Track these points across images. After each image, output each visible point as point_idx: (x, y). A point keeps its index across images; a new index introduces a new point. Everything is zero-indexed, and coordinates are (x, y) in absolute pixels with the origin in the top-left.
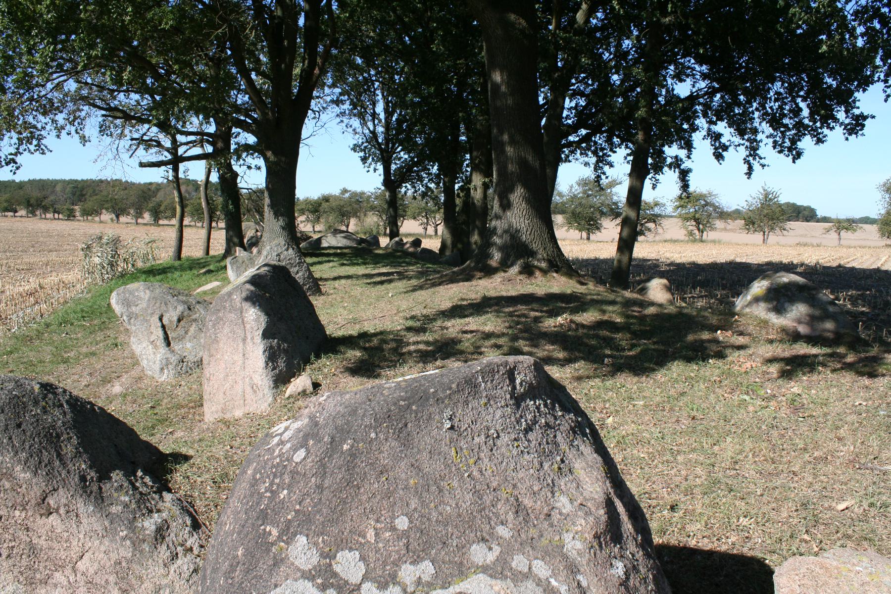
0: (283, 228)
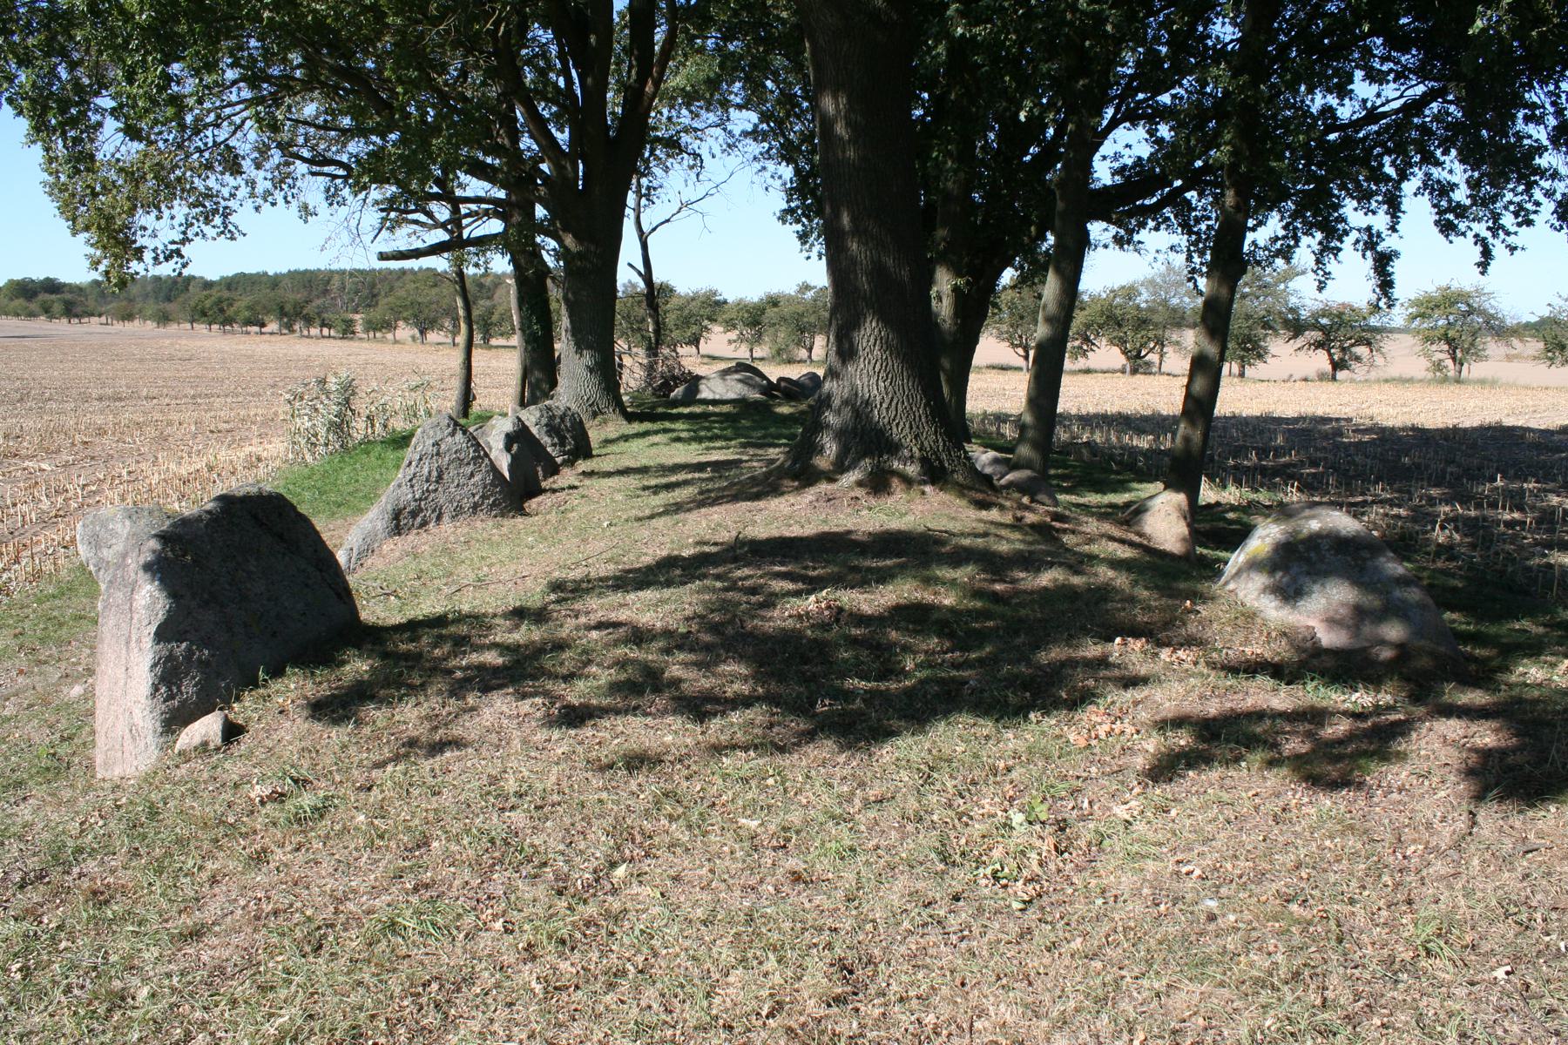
0: (591, 370)
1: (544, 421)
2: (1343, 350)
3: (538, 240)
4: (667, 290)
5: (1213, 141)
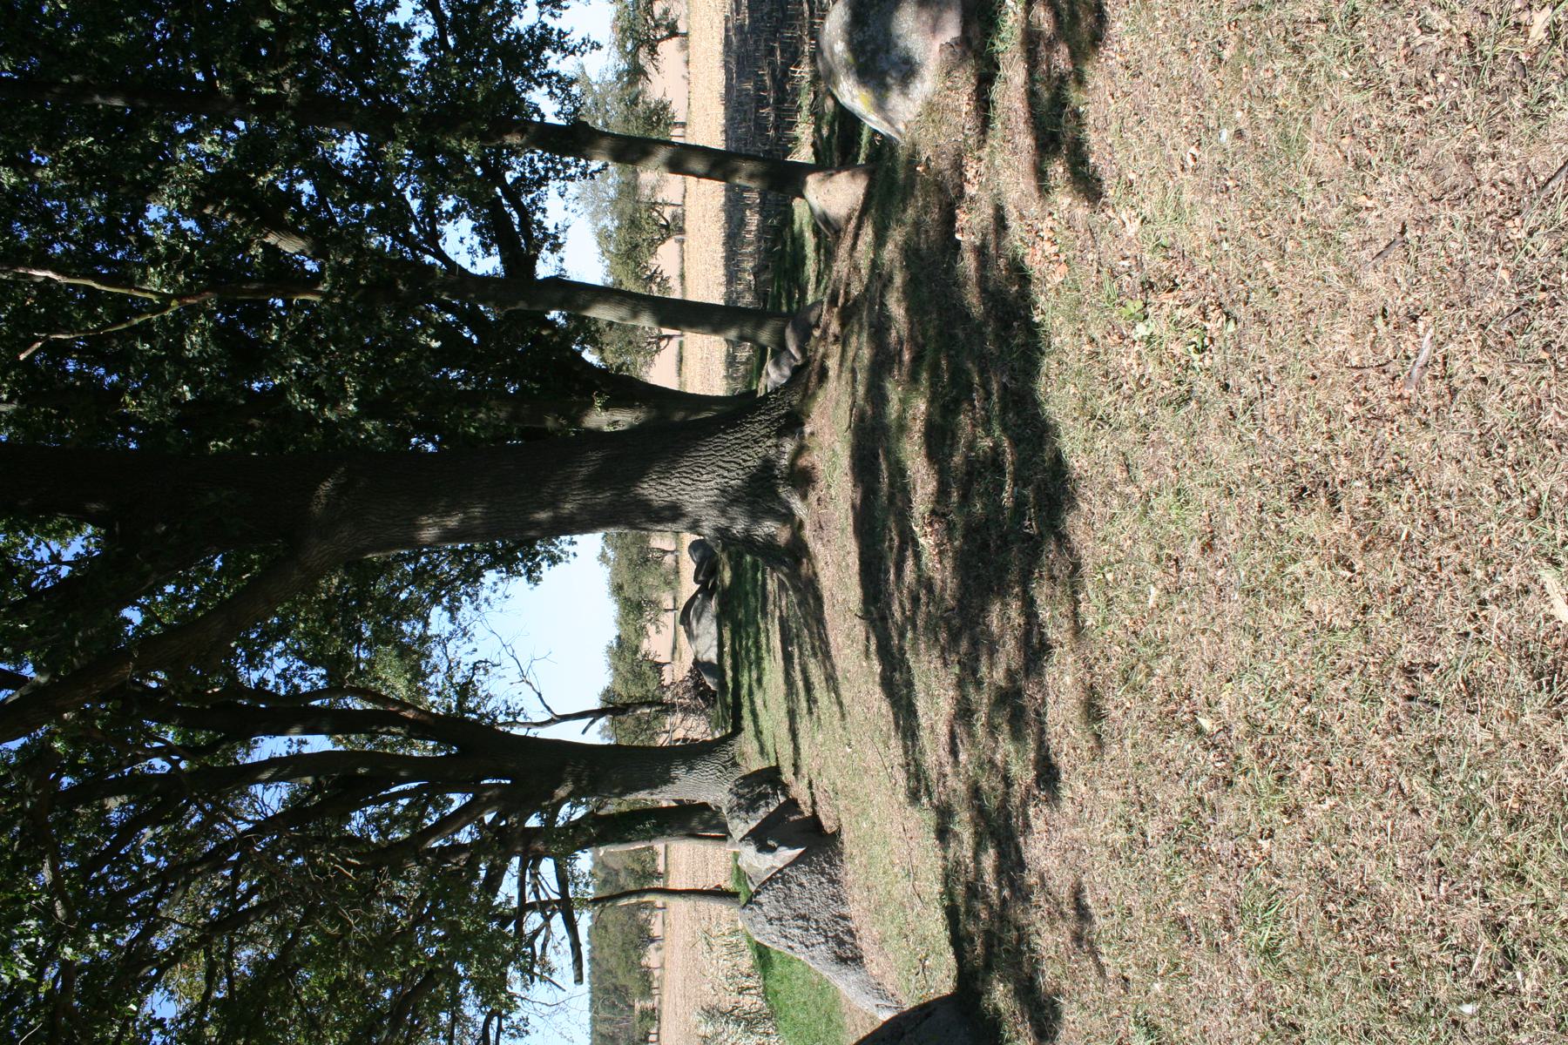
0: (691, 769)
1: (743, 815)
2: (657, 26)
3: (561, 823)
4: (607, 695)
5: (457, 157)
